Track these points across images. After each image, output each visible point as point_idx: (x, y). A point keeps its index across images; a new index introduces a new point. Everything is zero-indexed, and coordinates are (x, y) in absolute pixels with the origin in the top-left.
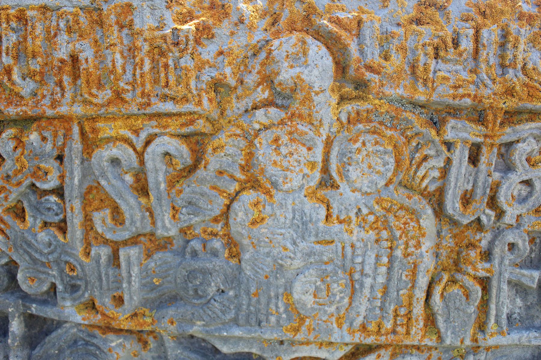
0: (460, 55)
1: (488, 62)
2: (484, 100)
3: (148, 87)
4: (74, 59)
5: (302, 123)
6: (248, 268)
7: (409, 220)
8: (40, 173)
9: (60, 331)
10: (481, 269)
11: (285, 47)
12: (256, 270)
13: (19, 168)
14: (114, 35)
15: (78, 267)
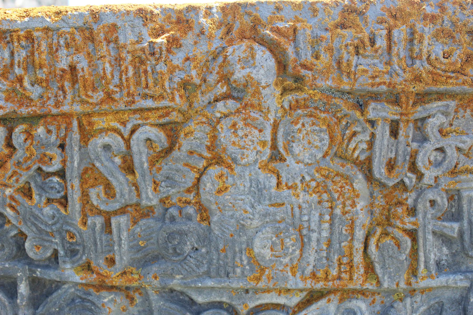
0: (376, 51)
1: (398, 55)
2: (396, 86)
3: (132, 88)
4: (73, 68)
5: (254, 111)
6: (217, 228)
7: (344, 185)
8: (46, 159)
9: (60, 291)
10: (408, 223)
11: (237, 53)
12: (223, 230)
13: (28, 156)
14: (103, 49)
15: (77, 234)
